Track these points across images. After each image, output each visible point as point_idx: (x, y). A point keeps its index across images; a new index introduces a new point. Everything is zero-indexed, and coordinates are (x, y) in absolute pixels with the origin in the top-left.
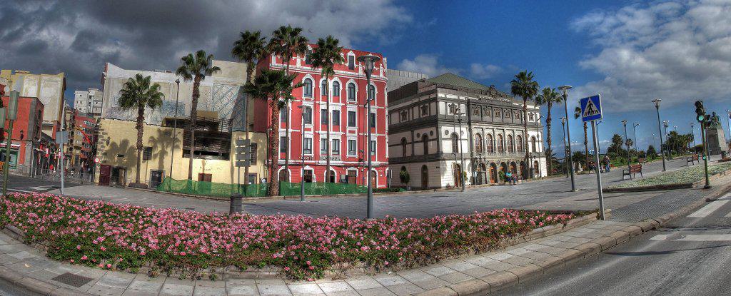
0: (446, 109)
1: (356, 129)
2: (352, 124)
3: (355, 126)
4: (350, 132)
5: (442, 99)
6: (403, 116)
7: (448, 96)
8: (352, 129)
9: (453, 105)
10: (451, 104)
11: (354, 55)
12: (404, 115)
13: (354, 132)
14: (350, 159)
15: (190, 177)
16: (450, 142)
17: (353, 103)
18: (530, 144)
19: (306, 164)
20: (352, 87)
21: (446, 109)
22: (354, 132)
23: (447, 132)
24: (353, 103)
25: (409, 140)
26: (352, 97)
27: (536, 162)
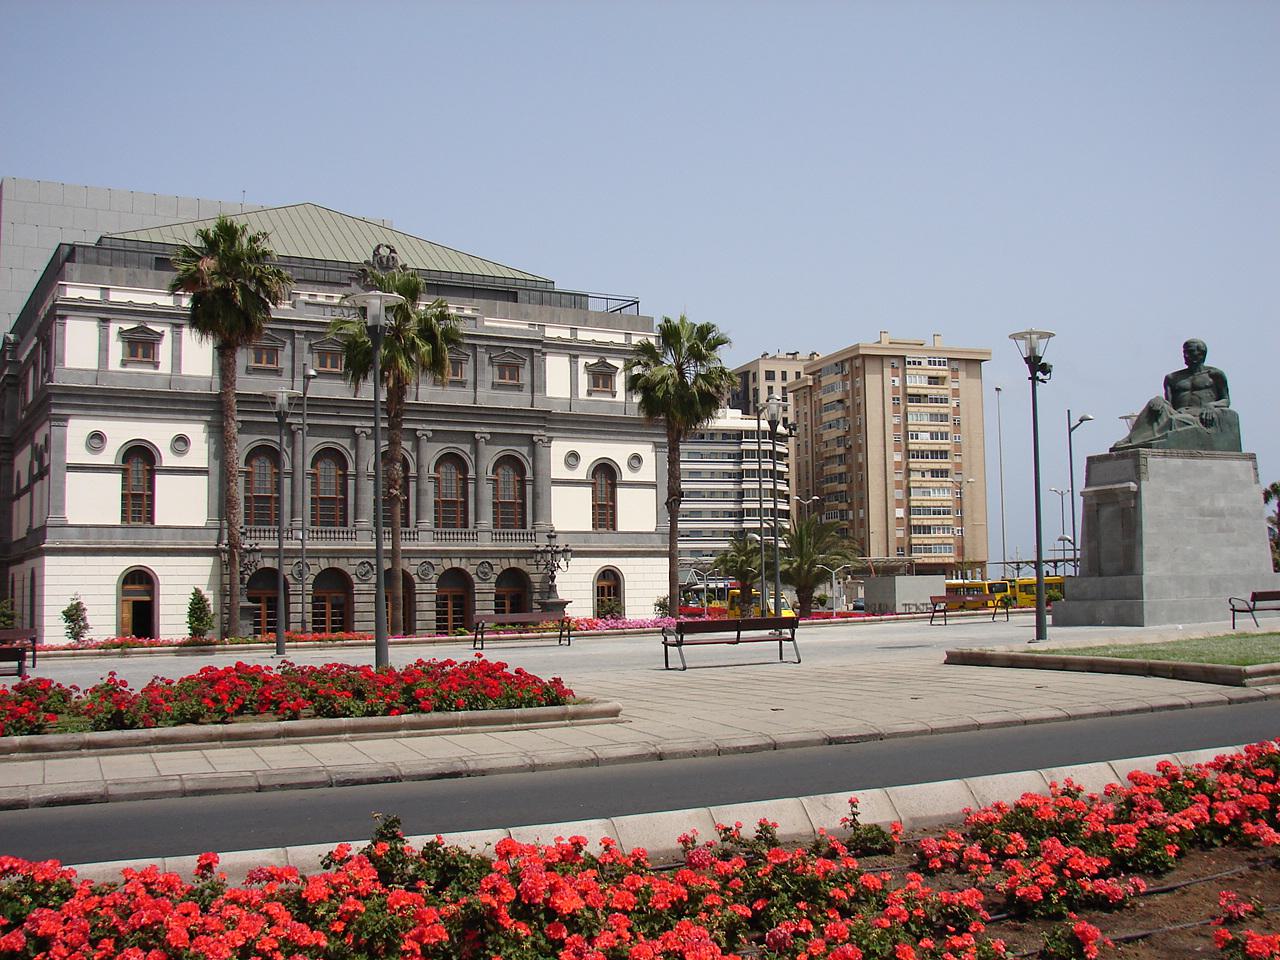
0: (104, 349)
5: (82, 309)
7: (117, 296)
16: (587, 493)
21: (104, 349)
23: (97, 439)
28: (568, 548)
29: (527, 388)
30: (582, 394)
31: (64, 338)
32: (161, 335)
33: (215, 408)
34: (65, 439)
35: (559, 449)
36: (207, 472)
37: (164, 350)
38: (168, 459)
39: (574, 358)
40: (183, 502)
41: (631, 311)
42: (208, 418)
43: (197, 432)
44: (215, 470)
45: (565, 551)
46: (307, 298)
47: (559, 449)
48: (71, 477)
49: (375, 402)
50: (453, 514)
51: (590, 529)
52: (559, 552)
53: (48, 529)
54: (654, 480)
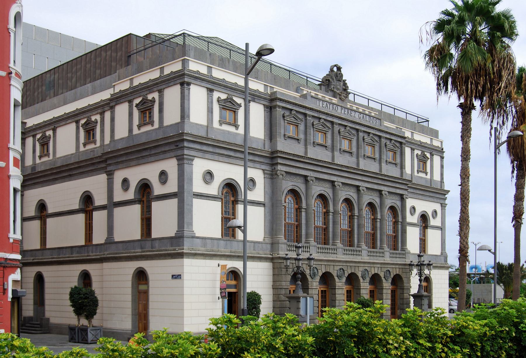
0: (210, 111)
12: (146, 109)
21: (210, 111)
23: (209, 176)
25: (100, 199)
28: (412, 263)
29: (302, 142)
30: (136, 131)
31: (189, 100)
32: (240, 106)
33: (272, 160)
34: (192, 173)
35: (199, 166)
36: (264, 204)
37: (241, 113)
38: (158, 189)
39: (210, 91)
40: (255, 223)
41: (425, 124)
42: (264, 167)
43: (257, 174)
44: (268, 204)
45: (429, 265)
46: (314, 95)
47: (199, 166)
48: (197, 203)
49: (244, 147)
50: (325, 238)
51: (220, 237)
52: (425, 265)
53: (185, 239)
54: (263, 201)
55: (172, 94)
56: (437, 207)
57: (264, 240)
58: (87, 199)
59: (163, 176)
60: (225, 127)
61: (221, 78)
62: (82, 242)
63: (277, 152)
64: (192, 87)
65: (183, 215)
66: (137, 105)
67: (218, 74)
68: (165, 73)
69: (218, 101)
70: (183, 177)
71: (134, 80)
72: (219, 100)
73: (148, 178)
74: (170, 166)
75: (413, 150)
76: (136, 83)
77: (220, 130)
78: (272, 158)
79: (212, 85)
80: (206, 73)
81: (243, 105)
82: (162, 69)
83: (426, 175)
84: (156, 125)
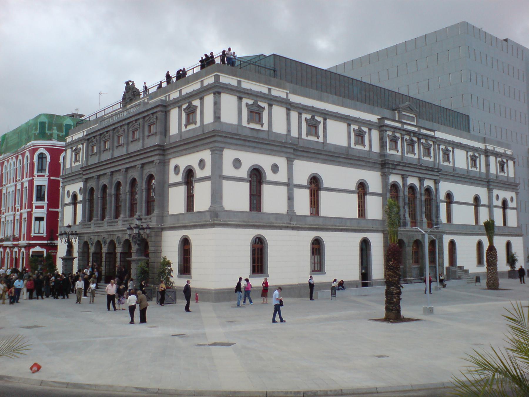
1: (45, 203)
2: (40, 198)
3: (43, 200)
4: (37, 207)
6: (188, 116)
8: (40, 203)
9: (255, 104)
10: (251, 102)
11: (47, 131)
12: (191, 111)
13: (42, 207)
14: (36, 238)
15: (289, 131)
17: (43, 176)
18: (443, 207)
19: (34, 245)
20: (41, 157)
22: (42, 207)
23: (237, 163)
24: (43, 176)
25: (484, 200)
26: (41, 169)
27: (185, 243)
30: (184, 129)
32: (264, 108)
35: (229, 155)
37: (321, 128)
39: (180, 107)
55: (209, 99)
56: (513, 194)
57: (287, 212)
58: (477, 199)
59: (202, 163)
60: (311, 138)
61: (259, 91)
62: (515, 211)
63: (490, 179)
64: (291, 112)
65: (216, 195)
66: (184, 110)
67: (246, 85)
68: (204, 85)
69: (246, 106)
70: (217, 164)
71: (182, 91)
72: (247, 104)
73: (206, 167)
74: (206, 155)
75: (300, 114)
76: (184, 93)
77: (306, 140)
78: (488, 182)
79: (240, 93)
80: (267, 93)
81: (322, 122)
82: (202, 82)
83: (318, 138)
84: (198, 124)
